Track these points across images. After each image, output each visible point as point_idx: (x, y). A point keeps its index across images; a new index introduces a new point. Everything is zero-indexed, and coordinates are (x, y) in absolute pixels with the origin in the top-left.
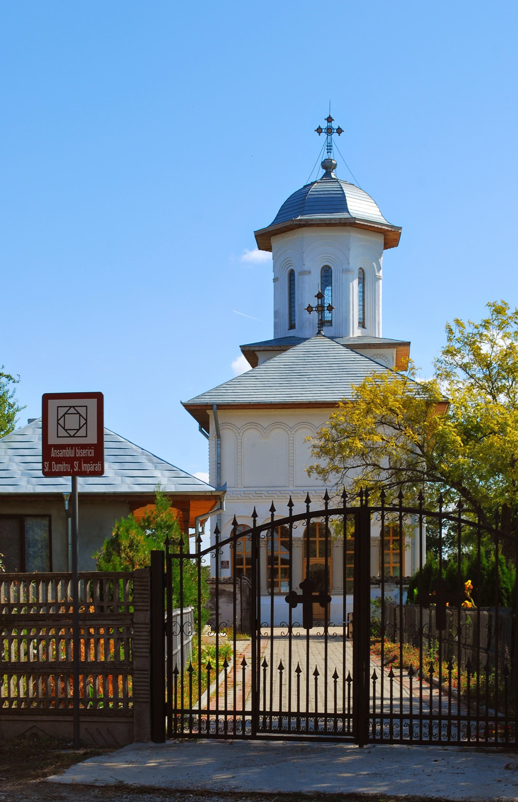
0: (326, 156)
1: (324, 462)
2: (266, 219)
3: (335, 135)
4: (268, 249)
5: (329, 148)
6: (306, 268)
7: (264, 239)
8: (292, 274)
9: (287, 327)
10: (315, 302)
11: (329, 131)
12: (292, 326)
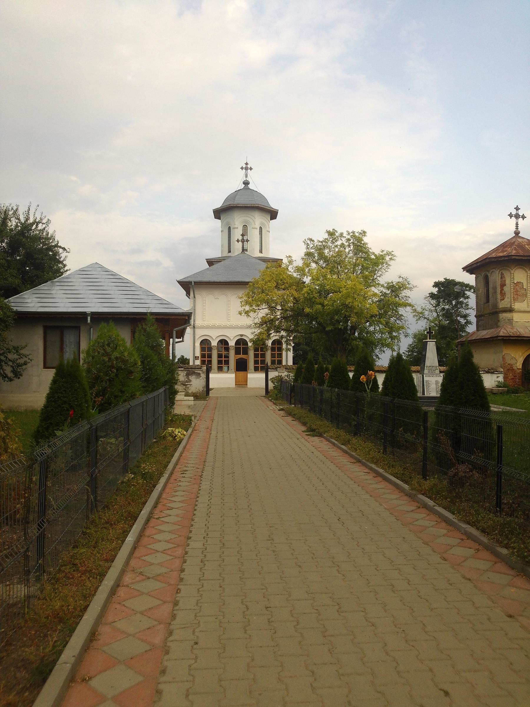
0: (245, 179)
1: (247, 308)
2: (218, 205)
3: (249, 171)
4: (219, 218)
5: (246, 176)
6: (236, 226)
7: (218, 213)
8: (229, 228)
9: (227, 252)
10: (240, 238)
11: (246, 169)
12: (230, 252)
